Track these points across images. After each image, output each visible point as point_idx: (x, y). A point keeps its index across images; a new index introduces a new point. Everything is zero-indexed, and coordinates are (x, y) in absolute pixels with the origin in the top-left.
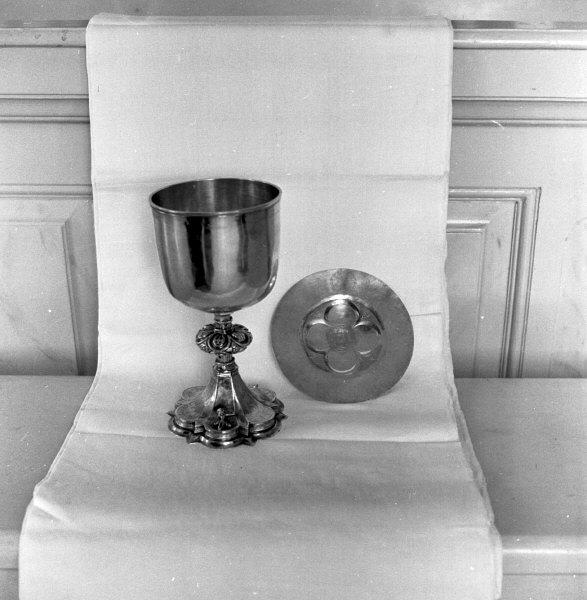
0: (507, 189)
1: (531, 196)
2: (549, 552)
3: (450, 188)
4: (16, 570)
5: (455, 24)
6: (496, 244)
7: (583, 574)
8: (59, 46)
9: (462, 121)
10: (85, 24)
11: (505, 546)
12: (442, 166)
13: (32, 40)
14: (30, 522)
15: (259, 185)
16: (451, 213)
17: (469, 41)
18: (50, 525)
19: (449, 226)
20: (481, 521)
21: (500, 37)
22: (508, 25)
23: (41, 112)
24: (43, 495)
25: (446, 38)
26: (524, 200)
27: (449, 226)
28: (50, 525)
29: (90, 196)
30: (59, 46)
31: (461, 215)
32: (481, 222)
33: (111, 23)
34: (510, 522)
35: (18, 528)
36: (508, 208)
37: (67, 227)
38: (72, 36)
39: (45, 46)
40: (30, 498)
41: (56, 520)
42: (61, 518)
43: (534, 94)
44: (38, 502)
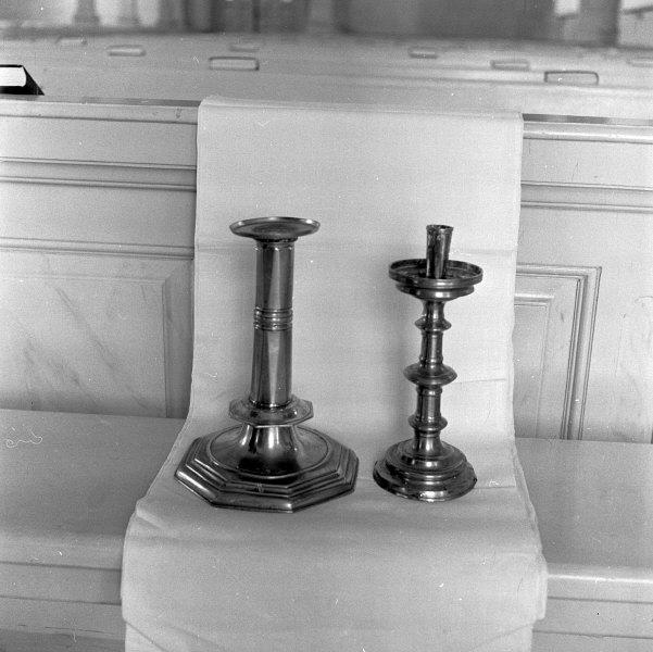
0: (540, 265)
1: (593, 274)
2: (581, 578)
3: (519, 264)
4: (119, 571)
5: (527, 117)
6: (559, 317)
7: (647, 603)
8: (175, 122)
9: (606, 207)
10: (197, 104)
11: (551, 570)
12: (514, 244)
13: (150, 116)
14: (133, 529)
15: (472, 266)
16: (518, 287)
17: (538, 132)
18: (151, 532)
19: (516, 299)
20: (531, 548)
21: (566, 130)
22: (602, 120)
23: (74, 177)
24: (144, 508)
25: (518, 128)
26: (586, 278)
27: (516, 299)
28: (151, 532)
29: (191, 257)
30: (175, 122)
31: (526, 290)
32: (546, 297)
33: (224, 104)
34: (558, 549)
35: (123, 534)
36: (570, 286)
37: (166, 288)
38: (186, 114)
39: (96, 119)
40: (134, 510)
41: (155, 527)
42: (159, 526)
43: (598, 181)
44: (139, 513)
